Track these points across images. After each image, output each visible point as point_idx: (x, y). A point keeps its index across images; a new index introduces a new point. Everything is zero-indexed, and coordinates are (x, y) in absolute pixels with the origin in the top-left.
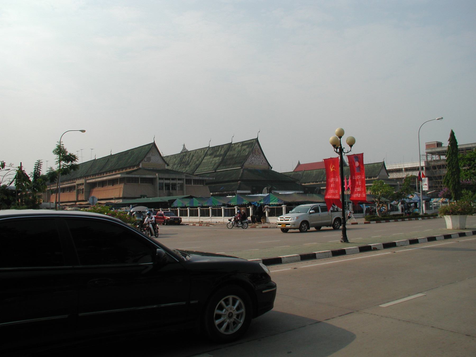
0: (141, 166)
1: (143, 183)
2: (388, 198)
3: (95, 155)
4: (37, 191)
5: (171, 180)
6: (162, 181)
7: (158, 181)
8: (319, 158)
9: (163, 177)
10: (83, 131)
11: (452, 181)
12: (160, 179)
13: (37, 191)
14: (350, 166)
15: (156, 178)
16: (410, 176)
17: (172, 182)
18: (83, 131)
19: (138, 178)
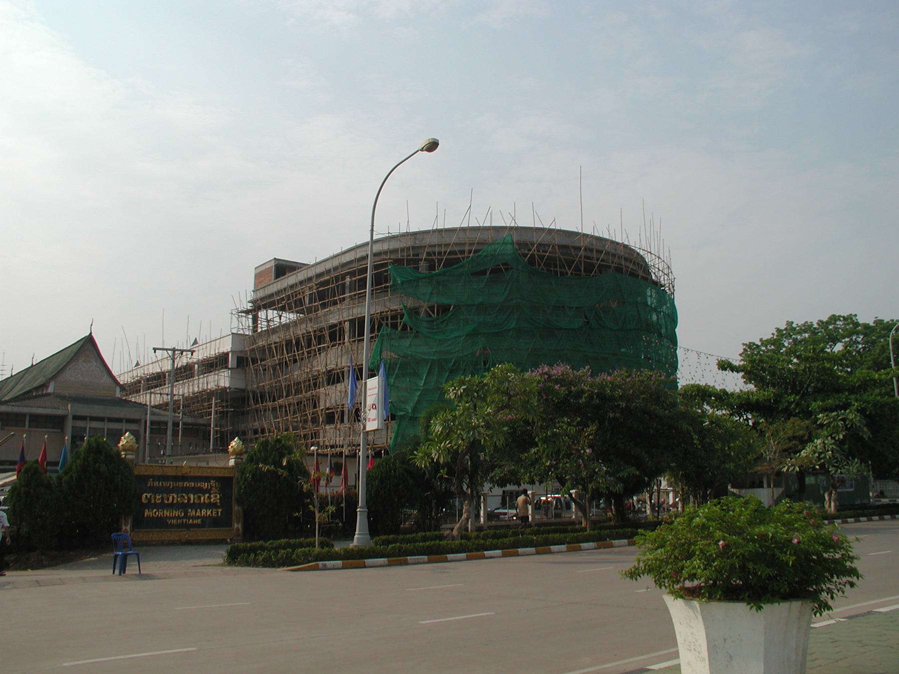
0: (51, 389)
1: (37, 427)
2: (756, 485)
3: (32, 356)
4: (797, 383)
5: (88, 420)
6: (80, 424)
7: (70, 424)
8: (769, 338)
9: (101, 415)
10: (432, 146)
11: (792, 552)
12: (75, 418)
13: (797, 383)
14: (837, 411)
15: (68, 415)
16: (6, 516)
17: (106, 426)
18: (432, 146)
19: (24, 415)
